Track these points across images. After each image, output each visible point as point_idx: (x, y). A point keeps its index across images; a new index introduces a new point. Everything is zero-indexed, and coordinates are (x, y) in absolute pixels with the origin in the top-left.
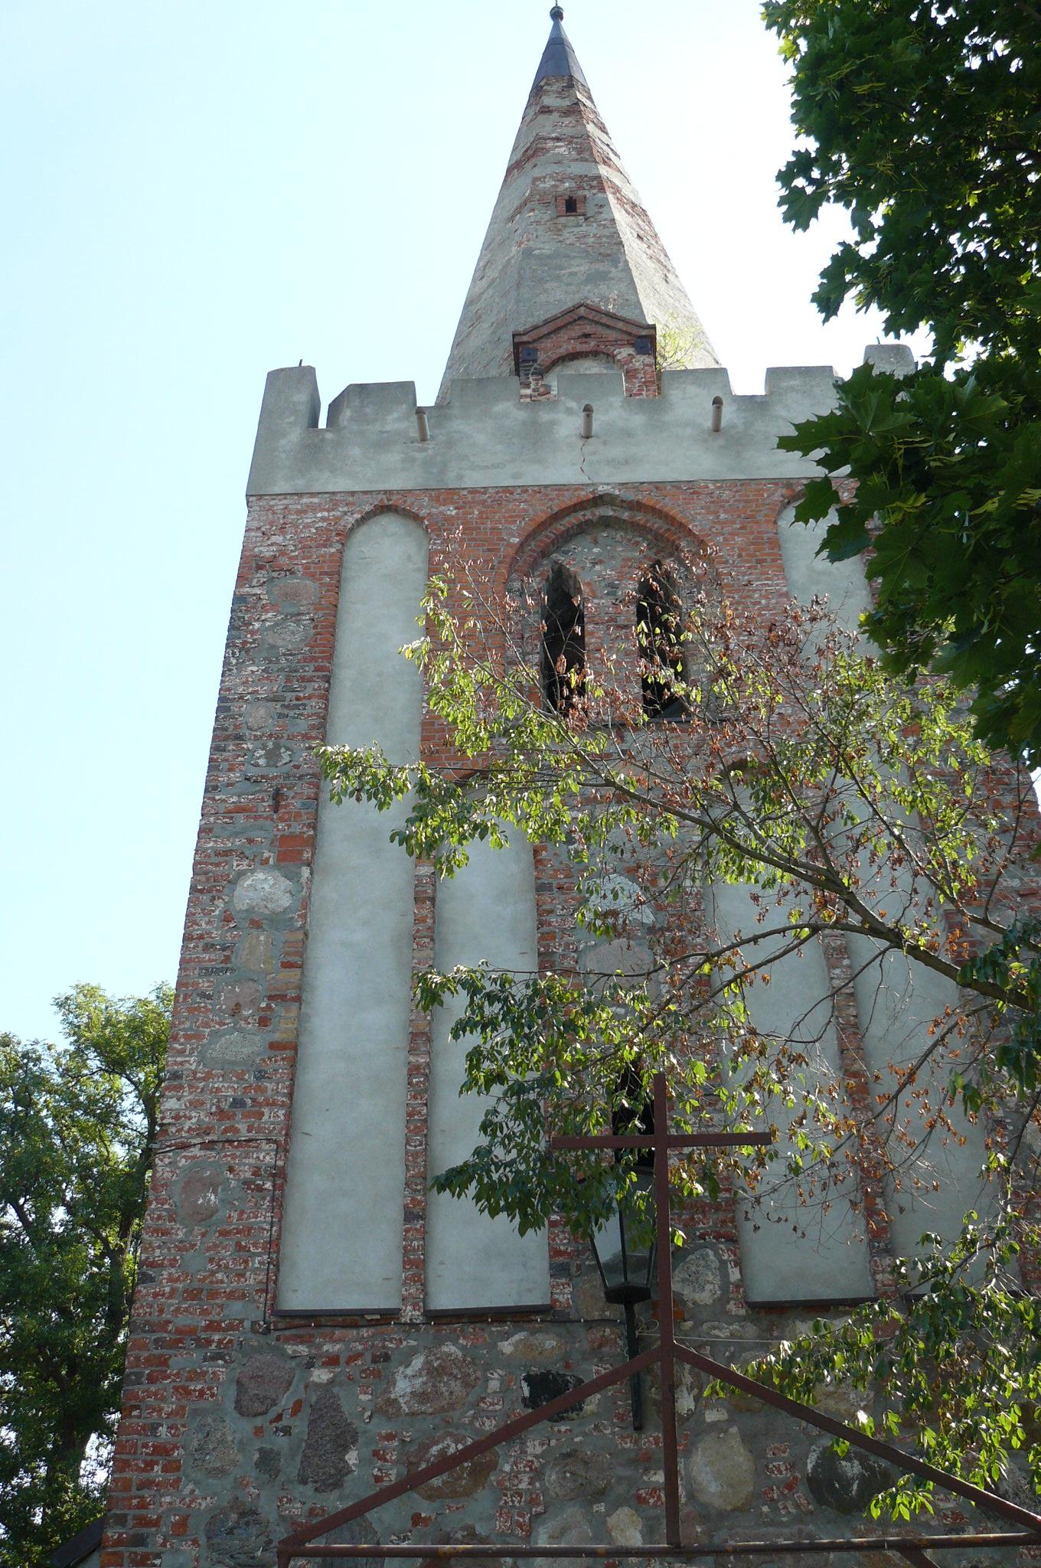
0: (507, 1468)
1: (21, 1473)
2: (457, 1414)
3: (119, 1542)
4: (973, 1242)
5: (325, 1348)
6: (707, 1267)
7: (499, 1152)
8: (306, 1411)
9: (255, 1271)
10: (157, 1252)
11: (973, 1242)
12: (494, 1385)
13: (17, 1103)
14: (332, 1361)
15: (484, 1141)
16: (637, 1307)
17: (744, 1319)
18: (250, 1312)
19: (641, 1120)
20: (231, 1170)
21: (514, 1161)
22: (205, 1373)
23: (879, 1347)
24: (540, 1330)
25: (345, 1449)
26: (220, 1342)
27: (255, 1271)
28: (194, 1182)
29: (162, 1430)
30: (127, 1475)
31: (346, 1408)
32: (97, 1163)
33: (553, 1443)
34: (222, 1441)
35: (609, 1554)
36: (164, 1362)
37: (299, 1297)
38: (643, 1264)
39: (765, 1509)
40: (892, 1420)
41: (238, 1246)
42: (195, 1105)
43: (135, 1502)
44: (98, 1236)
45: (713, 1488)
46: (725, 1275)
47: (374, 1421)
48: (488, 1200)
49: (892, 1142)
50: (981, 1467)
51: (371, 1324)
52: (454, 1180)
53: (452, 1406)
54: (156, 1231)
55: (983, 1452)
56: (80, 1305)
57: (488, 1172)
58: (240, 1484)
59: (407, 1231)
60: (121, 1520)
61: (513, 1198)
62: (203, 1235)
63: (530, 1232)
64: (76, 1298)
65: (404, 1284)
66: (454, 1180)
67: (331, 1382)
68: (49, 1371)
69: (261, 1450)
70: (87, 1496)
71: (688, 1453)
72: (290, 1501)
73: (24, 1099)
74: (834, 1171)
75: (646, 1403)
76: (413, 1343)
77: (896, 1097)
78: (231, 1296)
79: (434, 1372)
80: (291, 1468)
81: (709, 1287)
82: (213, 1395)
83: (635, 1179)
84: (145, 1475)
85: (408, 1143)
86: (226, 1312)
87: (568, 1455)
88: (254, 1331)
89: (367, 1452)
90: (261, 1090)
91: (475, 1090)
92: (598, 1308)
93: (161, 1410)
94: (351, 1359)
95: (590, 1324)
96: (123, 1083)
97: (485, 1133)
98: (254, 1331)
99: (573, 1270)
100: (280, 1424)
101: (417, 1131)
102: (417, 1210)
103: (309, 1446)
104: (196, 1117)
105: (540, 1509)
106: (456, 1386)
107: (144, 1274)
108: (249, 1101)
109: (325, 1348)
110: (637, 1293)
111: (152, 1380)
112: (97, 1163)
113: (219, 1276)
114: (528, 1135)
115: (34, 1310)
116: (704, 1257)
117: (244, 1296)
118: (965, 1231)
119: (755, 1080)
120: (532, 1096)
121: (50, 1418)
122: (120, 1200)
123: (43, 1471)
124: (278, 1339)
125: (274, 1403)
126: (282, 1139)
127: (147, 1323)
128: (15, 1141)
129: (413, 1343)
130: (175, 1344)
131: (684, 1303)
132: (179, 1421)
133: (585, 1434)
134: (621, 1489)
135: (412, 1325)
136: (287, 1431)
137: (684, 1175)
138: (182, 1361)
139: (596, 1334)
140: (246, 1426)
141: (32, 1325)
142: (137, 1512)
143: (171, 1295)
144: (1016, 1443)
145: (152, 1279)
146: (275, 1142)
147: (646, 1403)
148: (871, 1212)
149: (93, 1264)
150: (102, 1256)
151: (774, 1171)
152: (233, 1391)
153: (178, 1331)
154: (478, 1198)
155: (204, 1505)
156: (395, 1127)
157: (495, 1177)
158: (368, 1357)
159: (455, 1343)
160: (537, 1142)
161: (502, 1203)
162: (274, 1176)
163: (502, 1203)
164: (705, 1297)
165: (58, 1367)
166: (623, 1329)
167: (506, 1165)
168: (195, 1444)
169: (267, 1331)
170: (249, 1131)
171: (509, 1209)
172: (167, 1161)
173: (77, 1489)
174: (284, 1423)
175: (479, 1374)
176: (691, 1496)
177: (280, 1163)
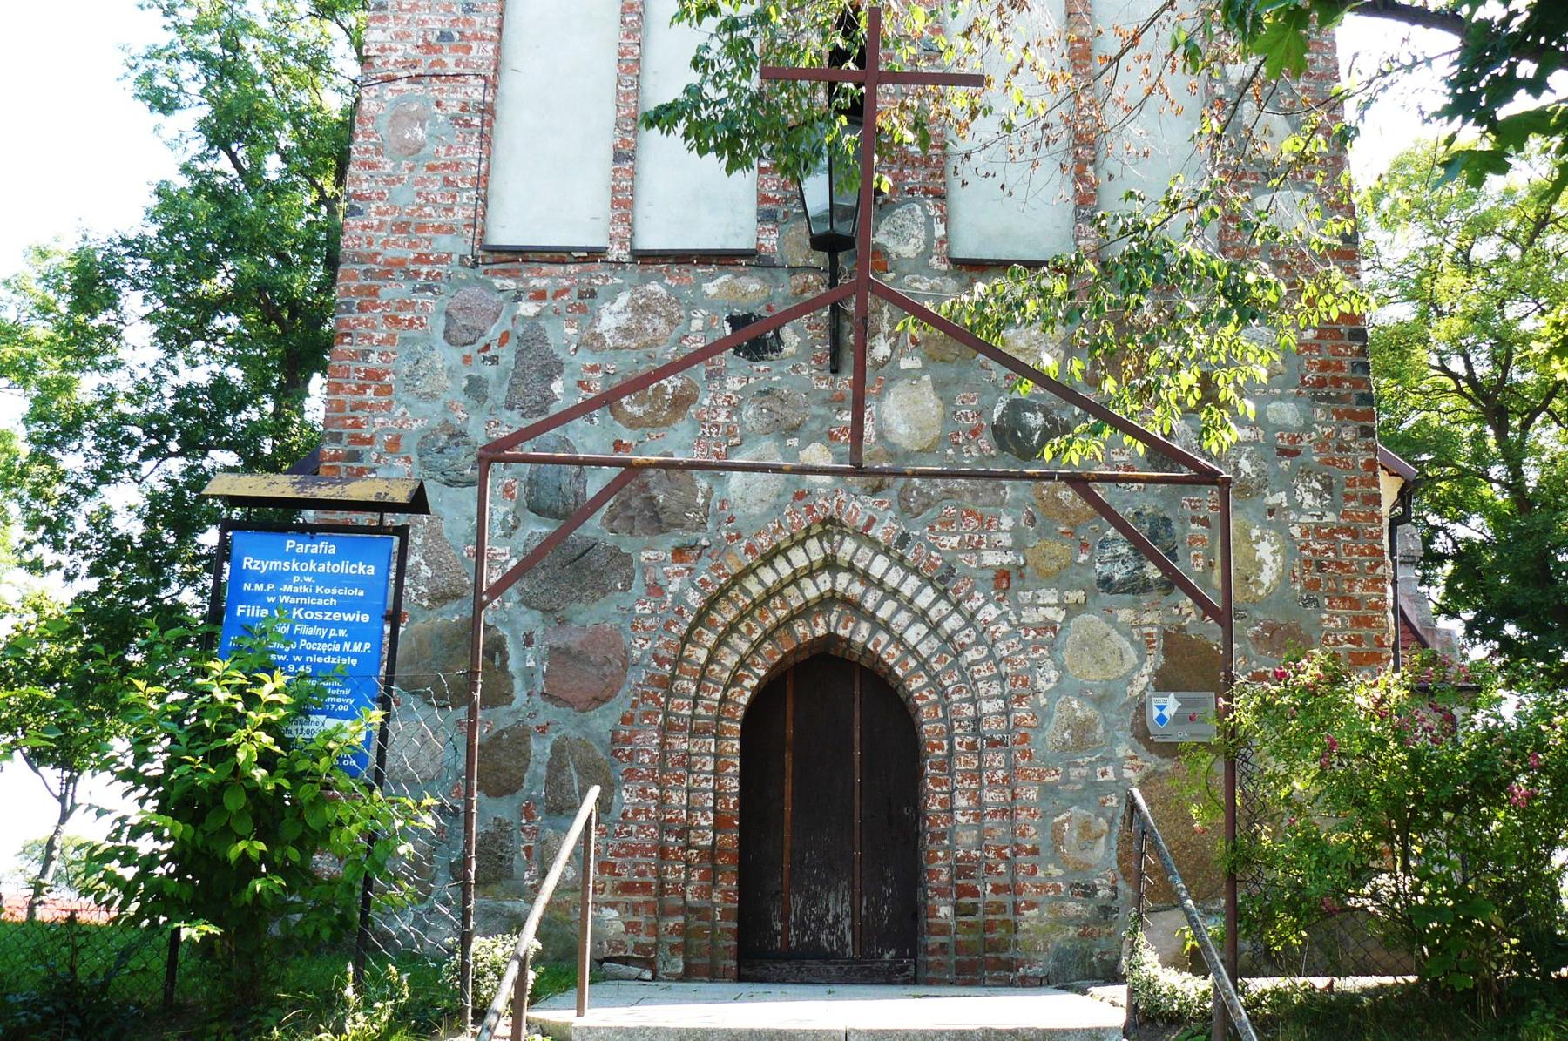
0: (706, 402)
1: (249, 408)
2: (659, 350)
3: (336, 457)
4: (1176, 203)
5: (532, 283)
6: (913, 221)
7: (709, 91)
8: (513, 341)
9: (463, 206)
10: (365, 186)
11: (1176, 203)
12: (697, 324)
13: (224, 46)
14: (540, 295)
15: (694, 77)
16: (840, 256)
17: (945, 273)
18: (462, 245)
19: (856, 63)
20: (438, 104)
21: (723, 101)
22: (413, 304)
23: (1071, 295)
24: (744, 274)
25: (551, 378)
26: (428, 274)
27: (463, 206)
28: (399, 116)
29: (374, 357)
30: (342, 397)
31: (551, 341)
32: (310, 111)
33: (752, 380)
34: (431, 368)
35: (794, 470)
36: (374, 292)
37: (504, 233)
38: (850, 213)
39: (950, 451)
40: (1077, 365)
41: (446, 180)
42: (401, 37)
43: (349, 422)
44: (313, 184)
45: (903, 430)
46: (930, 231)
47: (580, 352)
48: (697, 139)
49: (1109, 108)
50: (1153, 421)
51: (578, 261)
52: (662, 117)
53: (655, 343)
54: (363, 164)
55: (1159, 408)
56: (299, 252)
57: (698, 108)
58: (449, 408)
59: (616, 171)
60: (337, 438)
61: (727, 139)
62: (411, 169)
63: (738, 174)
64: (294, 245)
65: (612, 223)
66: (662, 117)
67: (538, 316)
68: (270, 314)
69: (469, 377)
70: (313, 430)
71: (880, 397)
72: (497, 425)
73: (230, 43)
74: (1047, 131)
75: (843, 348)
76: (619, 281)
77: (1117, 59)
78: (439, 229)
79: (641, 309)
80: (499, 395)
81: (913, 241)
82: (422, 325)
83: (845, 123)
84: (358, 398)
85: (619, 83)
86: (435, 245)
87: (766, 393)
88: (462, 264)
89: (572, 382)
90: (467, 22)
91: (687, 21)
92: (802, 254)
93: (372, 337)
94: (557, 294)
95: (793, 270)
96: (331, 27)
97: (696, 68)
98: (462, 264)
99: (780, 216)
100: (488, 354)
101: (629, 70)
102: (625, 151)
103: (516, 375)
104: (405, 50)
105: (736, 441)
106: (660, 324)
107: (352, 207)
108: (456, 35)
109: (532, 283)
110: (838, 243)
111: (362, 309)
112: (310, 111)
113: (428, 210)
114: (739, 73)
115: (252, 254)
116: (911, 211)
117: (452, 230)
118: (1169, 191)
119: (975, 26)
120: (746, 33)
121: (274, 359)
122: (332, 149)
123: (270, 407)
124: (486, 273)
125: (482, 334)
126: (491, 74)
127: (356, 254)
128: (224, 86)
129: (619, 281)
130: (385, 275)
131: (889, 255)
132: (389, 348)
133: (782, 374)
134: (814, 426)
135: (619, 263)
136: (494, 360)
137: (895, 121)
138: (391, 291)
139: (799, 280)
140: (455, 355)
141: (252, 270)
142: (353, 431)
143: (380, 228)
144: (1191, 402)
145: (360, 212)
146: (484, 77)
147: (843, 348)
148: (1080, 177)
149: (309, 211)
150: (319, 204)
151: (986, 127)
152: (441, 322)
153: (388, 263)
154: (686, 136)
155: (415, 425)
156: (607, 67)
157: (704, 114)
158: (575, 292)
159: (660, 281)
160: (748, 79)
161: (711, 143)
162: (483, 111)
163: (711, 143)
164: (908, 250)
165: (280, 310)
166: (826, 277)
167: (717, 103)
168: (406, 370)
169: (475, 265)
170: (457, 65)
171: (718, 149)
172: (373, 94)
173: (303, 424)
174: (491, 352)
175: (683, 313)
176: (881, 436)
177: (489, 99)
